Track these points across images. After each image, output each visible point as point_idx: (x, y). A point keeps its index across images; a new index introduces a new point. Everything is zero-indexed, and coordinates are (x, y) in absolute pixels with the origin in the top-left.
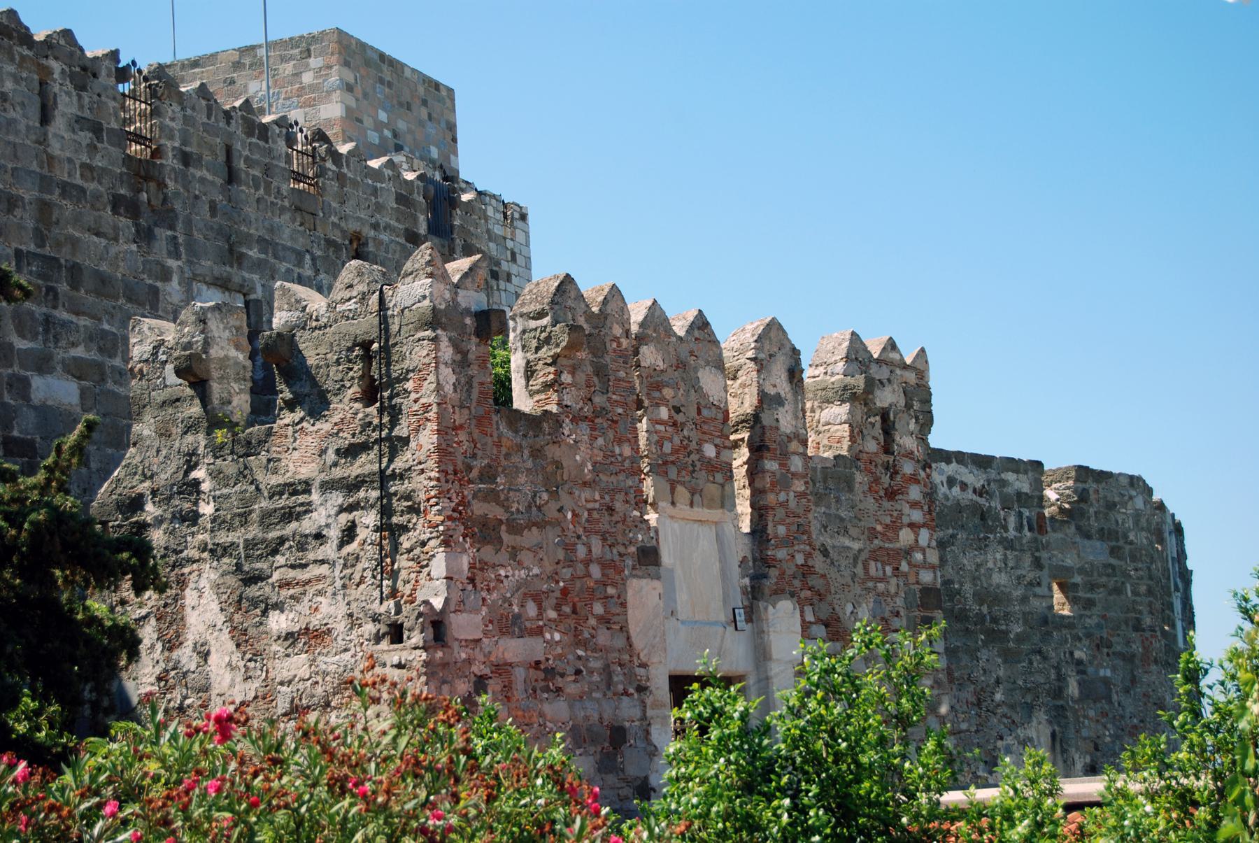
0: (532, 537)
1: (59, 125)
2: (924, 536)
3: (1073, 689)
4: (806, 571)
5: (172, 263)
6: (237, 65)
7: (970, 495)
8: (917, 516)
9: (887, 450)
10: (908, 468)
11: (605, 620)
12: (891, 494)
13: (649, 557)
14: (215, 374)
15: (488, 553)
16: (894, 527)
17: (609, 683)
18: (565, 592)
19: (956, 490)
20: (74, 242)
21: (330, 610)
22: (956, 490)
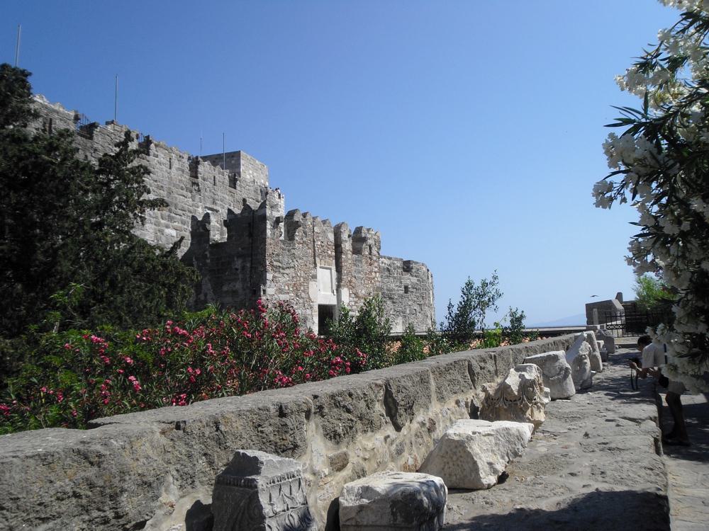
0: (287, 271)
1: (173, 169)
2: (378, 274)
3: (408, 312)
4: (350, 282)
5: (200, 204)
6: (216, 159)
7: (386, 266)
8: (376, 269)
9: (370, 254)
10: (375, 258)
11: (303, 291)
12: (371, 265)
13: (314, 277)
14: (212, 229)
15: (276, 275)
16: (371, 272)
17: (304, 306)
18: (295, 284)
19: (383, 265)
20: (176, 198)
21: (238, 286)
22: (383, 265)
